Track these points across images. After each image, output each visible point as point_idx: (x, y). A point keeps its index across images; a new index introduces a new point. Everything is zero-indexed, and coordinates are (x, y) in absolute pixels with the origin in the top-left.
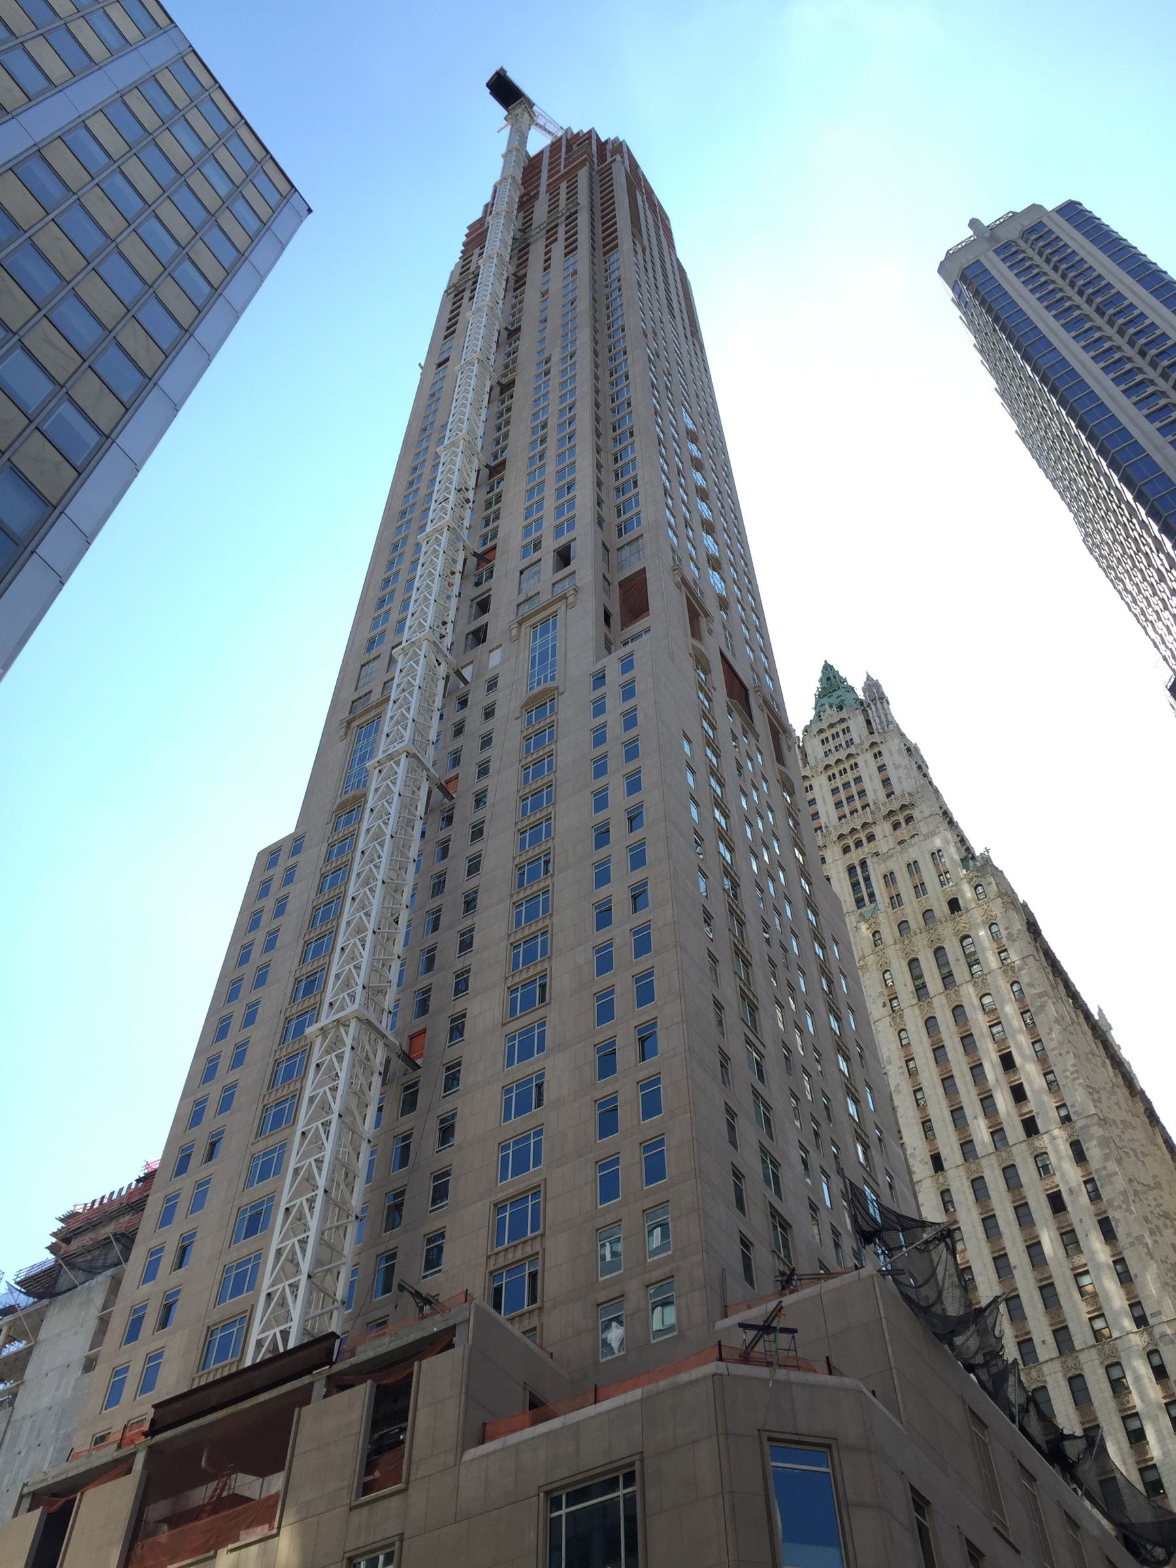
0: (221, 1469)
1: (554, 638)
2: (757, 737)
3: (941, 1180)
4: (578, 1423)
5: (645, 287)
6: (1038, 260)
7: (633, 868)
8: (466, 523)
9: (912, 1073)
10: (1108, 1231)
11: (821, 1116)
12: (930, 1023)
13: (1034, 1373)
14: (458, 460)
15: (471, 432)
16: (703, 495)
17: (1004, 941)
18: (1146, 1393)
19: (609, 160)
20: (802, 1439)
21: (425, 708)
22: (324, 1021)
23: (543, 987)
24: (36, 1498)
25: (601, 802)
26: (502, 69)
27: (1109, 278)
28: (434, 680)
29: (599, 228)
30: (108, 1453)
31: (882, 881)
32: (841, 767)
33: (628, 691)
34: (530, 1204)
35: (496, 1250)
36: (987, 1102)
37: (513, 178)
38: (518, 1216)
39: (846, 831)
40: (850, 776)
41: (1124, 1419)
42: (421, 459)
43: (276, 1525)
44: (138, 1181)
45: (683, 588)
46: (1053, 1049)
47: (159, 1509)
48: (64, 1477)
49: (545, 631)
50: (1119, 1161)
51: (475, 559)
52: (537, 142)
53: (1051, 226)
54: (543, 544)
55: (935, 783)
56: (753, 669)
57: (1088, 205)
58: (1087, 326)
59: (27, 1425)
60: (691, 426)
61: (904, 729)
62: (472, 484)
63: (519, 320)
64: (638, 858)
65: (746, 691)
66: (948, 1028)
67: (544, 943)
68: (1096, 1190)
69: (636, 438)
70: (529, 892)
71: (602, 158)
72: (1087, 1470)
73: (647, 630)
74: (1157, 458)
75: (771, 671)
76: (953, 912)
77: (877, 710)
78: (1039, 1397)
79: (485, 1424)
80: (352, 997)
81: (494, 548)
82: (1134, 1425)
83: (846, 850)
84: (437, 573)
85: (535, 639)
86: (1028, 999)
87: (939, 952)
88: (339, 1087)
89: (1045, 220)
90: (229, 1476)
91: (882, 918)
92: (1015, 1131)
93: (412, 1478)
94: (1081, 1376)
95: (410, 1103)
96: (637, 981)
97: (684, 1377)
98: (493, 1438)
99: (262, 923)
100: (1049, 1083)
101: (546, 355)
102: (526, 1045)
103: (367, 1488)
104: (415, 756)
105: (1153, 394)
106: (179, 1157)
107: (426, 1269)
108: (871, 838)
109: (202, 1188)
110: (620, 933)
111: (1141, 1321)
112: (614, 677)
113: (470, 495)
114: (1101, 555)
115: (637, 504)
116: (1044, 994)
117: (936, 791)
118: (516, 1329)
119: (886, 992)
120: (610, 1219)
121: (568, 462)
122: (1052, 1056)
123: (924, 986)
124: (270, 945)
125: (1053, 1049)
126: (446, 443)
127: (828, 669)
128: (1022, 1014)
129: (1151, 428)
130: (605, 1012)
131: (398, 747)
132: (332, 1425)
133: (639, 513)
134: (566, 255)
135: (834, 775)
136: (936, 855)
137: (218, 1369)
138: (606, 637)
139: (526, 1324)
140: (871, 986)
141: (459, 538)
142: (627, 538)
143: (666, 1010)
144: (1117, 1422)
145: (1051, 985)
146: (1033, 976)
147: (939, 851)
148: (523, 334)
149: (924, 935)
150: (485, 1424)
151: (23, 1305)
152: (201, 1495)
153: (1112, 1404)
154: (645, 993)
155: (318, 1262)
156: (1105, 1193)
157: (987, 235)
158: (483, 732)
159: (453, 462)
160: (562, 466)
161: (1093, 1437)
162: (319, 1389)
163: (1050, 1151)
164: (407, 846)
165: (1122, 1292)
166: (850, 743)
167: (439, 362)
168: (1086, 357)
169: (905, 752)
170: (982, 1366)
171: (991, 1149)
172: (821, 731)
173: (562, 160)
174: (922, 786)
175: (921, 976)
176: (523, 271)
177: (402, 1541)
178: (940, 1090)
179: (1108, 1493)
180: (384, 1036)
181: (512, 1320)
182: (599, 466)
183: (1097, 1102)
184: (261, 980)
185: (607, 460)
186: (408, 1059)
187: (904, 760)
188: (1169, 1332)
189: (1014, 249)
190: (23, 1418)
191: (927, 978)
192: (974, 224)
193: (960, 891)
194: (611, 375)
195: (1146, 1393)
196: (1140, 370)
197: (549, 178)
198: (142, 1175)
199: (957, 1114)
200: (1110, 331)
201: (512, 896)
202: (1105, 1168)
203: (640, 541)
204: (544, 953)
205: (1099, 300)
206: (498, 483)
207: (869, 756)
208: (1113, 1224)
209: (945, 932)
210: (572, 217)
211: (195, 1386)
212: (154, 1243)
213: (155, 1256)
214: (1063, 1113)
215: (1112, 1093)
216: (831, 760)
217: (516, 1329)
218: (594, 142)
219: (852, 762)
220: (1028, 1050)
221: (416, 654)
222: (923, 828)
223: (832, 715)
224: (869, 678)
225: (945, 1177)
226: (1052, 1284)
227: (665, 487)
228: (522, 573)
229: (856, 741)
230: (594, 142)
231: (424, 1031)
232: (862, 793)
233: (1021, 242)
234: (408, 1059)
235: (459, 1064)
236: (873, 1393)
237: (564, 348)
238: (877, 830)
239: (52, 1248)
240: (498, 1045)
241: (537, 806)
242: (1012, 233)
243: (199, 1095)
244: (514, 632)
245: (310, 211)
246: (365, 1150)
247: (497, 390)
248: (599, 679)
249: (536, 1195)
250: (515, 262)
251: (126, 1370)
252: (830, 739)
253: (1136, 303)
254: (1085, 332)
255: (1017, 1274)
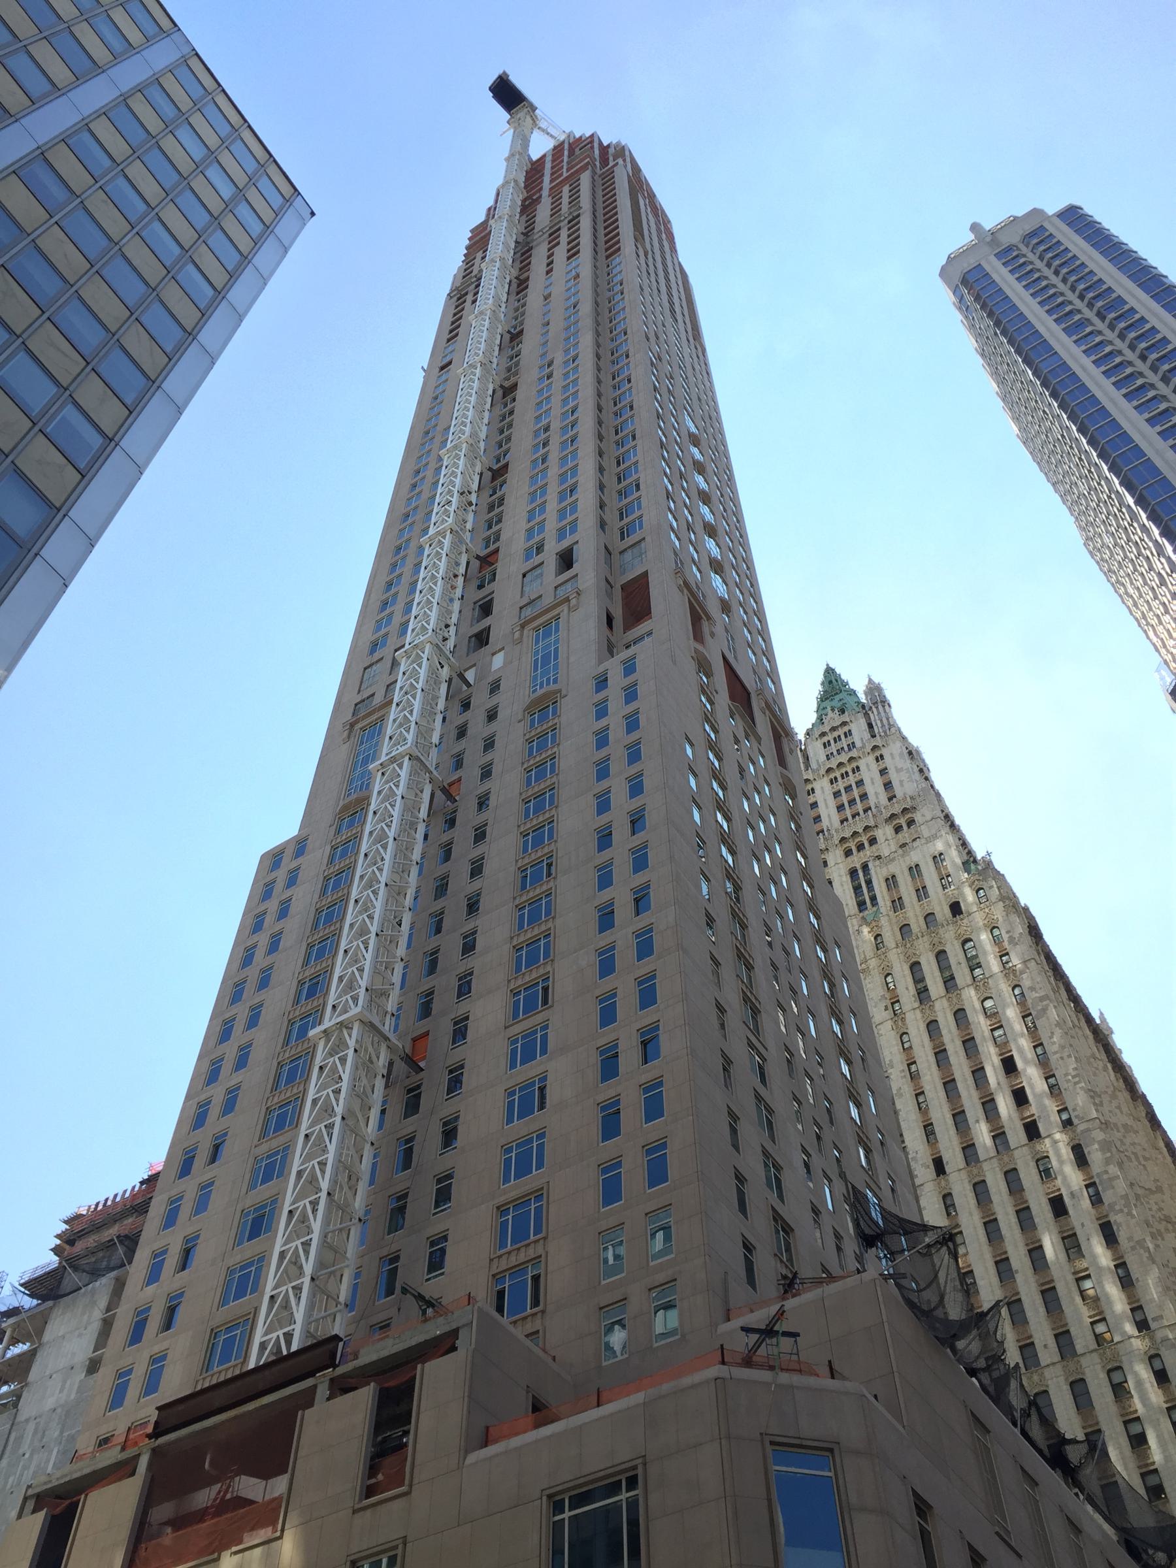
0: (223, 1473)
1: (556, 642)
2: (759, 740)
3: (943, 1183)
4: (580, 1426)
5: (647, 290)
6: (1039, 264)
7: (636, 871)
8: (469, 526)
9: (914, 1077)
10: (1109, 1235)
11: (824, 1120)
12: (932, 1027)
13: (1036, 1378)
14: (461, 463)
15: (474, 434)
16: (705, 498)
17: (1006, 944)
18: (1147, 1396)
19: (611, 164)
20: (805, 1443)
21: (428, 711)
22: (327, 1024)
23: (546, 990)
24: (40, 1500)
25: (603, 805)
26: (504, 73)
27: (1109, 282)
28: (437, 683)
29: (601, 232)
30: (112, 1456)
31: (884, 885)
32: (843, 771)
33: (631, 694)
34: (533, 1207)
35: (499, 1253)
36: (989, 1104)
37: (515, 181)
38: (521, 1219)
39: (847, 834)
40: (852, 780)
41: (1126, 1423)
42: (424, 462)
43: (279, 1527)
44: (142, 1183)
45: (685, 591)
46: (1056, 1053)
47: (163, 1512)
48: (67, 1479)
49: (547, 634)
50: (1120, 1165)
51: (478, 563)
52: (540, 146)
53: (1051, 230)
54: (546, 548)
55: (937, 786)
56: (755, 673)
57: (1089, 209)
58: (1088, 330)
59: (31, 1426)
60: (693, 429)
61: (906, 732)
62: (475, 487)
63: (522, 323)
64: (640, 862)
65: (749, 694)
66: (950, 1032)
67: (547, 945)
68: (1097, 1194)
69: (638, 441)
70: (531, 894)
71: (604, 161)
72: (1089, 1474)
73: (650, 634)
74: (1158, 463)
75: (774, 675)
76: (954, 916)
77: (879, 713)
78: (1041, 1401)
79: (487, 1428)
80: (355, 999)
81: (497, 551)
82: (1135, 1429)
83: (848, 853)
84: (439, 576)
85: (537, 642)
86: (1029, 1001)
87: (941, 955)
88: (340, 1085)
89: (1046, 225)
90: (232, 1478)
91: (884, 921)
92: (1016, 1136)
93: (415, 1481)
94: (1083, 1380)
95: (412, 1105)
96: (640, 984)
97: (687, 1381)
98: (496, 1441)
99: (266, 925)
100: (1051, 1087)
101: (549, 358)
102: (529, 1048)
103: (370, 1491)
104: (418, 759)
105: (1154, 398)
106: (183, 1160)
107: (429, 1272)
108: (873, 841)
109: (206, 1188)
110: (623, 936)
111: (1142, 1325)
112: (617, 680)
113: (473, 498)
114: (1102, 559)
115: (639, 508)
116: (1045, 998)
117: (938, 795)
118: (518, 1332)
119: (888, 996)
120: (612, 1222)
121: (570, 465)
122: (1053, 1059)
123: (926, 989)
124: (274, 947)
125: (1056, 1053)
126: (449, 445)
127: (829, 671)
128: (1023, 1017)
129: (1152, 432)
130: (608, 1015)
131: (401, 749)
132: (336, 1427)
133: (641, 516)
134: (569, 258)
135: (836, 778)
136: (938, 859)
137: (222, 1372)
138: (609, 640)
139: (529, 1327)
140: (873, 989)
141: (462, 541)
142: (629, 541)
143: (668, 1012)
144: (1120, 1428)
145: (1053, 989)
146: (1034, 979)
147: (941, 854)
148: (526, 337)
149: (925, 938)
150: (487, 1428)
151: (27, 1307)
152: (204, 1497)
153: (1113, 1408)
154: (647, 995)
155: (321, 1264)
156: (1107, 1197)
157: (988, 239)
158: (489, 705)
159: (452, 483)
160: (564, 469)
161: (1094, 1442)
162: (323, 1391)
163: (1051, 1155)
164: (410, 848)
165: (1123, 1297)
166: (851, 746)
167: (442, 366)
168: (1087, 361)
169: (906, 756)
170: (984, 1370)
171: (993, 1153)
172: (823, 734)
173: (565, 163)
174: (923, 789)
175: (923, 980)
176: (525, 275)
177: (405, 1544)
178: (942, 1094)
179: (1110, 1498)
180: (387, 1039)
181: (515, 1322)
182: (601, 470)
183: (1098, 1106)
184: (264, 982)
185: (609, 463)
186: (411, 1062)
187: (907, 763)
188: (1171, 1336)
189: (1015, 254)
190: (27, 1421)
191: (929, 982)
192: (975, 228)
193: (962, 894)
194: (614, 378)
195: (1147, 1396)
196: (1141, 374)
197: (551, 181)
198: (146, 1177)
199: (959, 1117)
200: (1110, 335)
201: (515, 898)
202: (1106, 1172)
203: (643, 544)
204: (547, 955)
205: (1100, 304)
206: (501, 486)
207: (871, 759)
208: (1115, 1228)
209: (947, 935)
210: (574, 221)
211: (199, 1388)
212: (157, 1246)
213: (159, 1256)
214: (1065, 1116)
215: (1114, 1097)
216: (833, 763)
217: (518, 1332)
218: (596, 145)
219: (854, 765)
220: (1030, 1054)
221: (419, 657)
222: (925, 832)
223: (834, 718)
224: (870, 681)
225: (947, 1181)
226: (1054, 1288)
227: (687, 521)
228: (524, 576)
229: (858, 744)
230: (596, 145)
231: (427, 1034)
232: (864, 796)
233: (1021, 246)
234: (411, 1062)
235: (462, 1067)
236: (876, 1397)
237: (567, 351)
238: (879, 834)
239: (56, 1250)
240: (501, 1048)
241: (539, 809)
242: (1007, 240)
243: (203, 1097)
244: (517, 635)
245: (313, 214)
246: (368, 1152)
247: (500, 393)
248: (602, 682)
249: (539, 1198)
250: (518, 265)
251: (130, 1372)
252: (832, 742)
253: (1137, 307)
254: (1086, 336)
255: (1019, 1278)
